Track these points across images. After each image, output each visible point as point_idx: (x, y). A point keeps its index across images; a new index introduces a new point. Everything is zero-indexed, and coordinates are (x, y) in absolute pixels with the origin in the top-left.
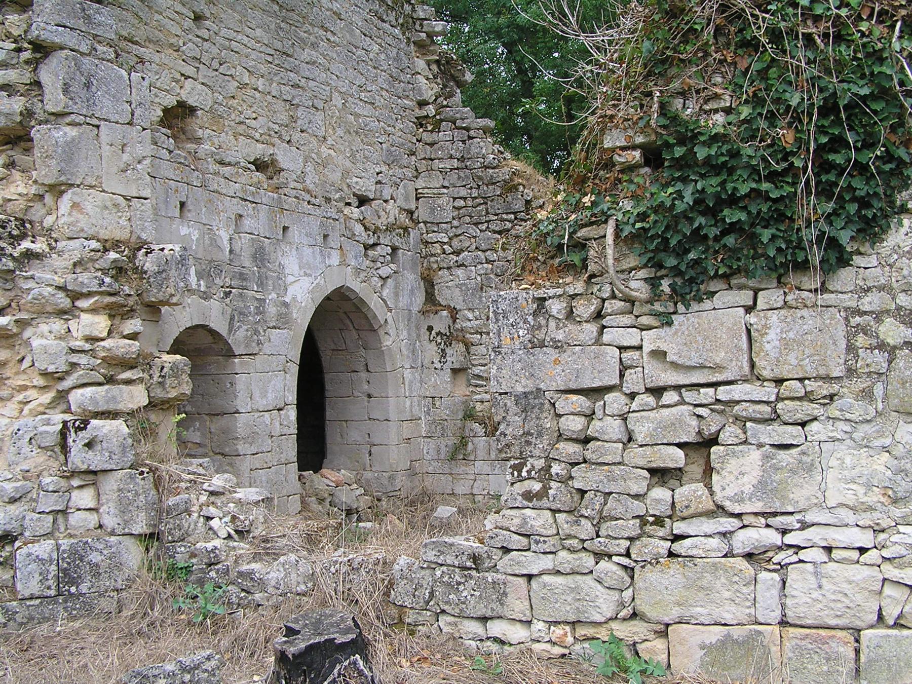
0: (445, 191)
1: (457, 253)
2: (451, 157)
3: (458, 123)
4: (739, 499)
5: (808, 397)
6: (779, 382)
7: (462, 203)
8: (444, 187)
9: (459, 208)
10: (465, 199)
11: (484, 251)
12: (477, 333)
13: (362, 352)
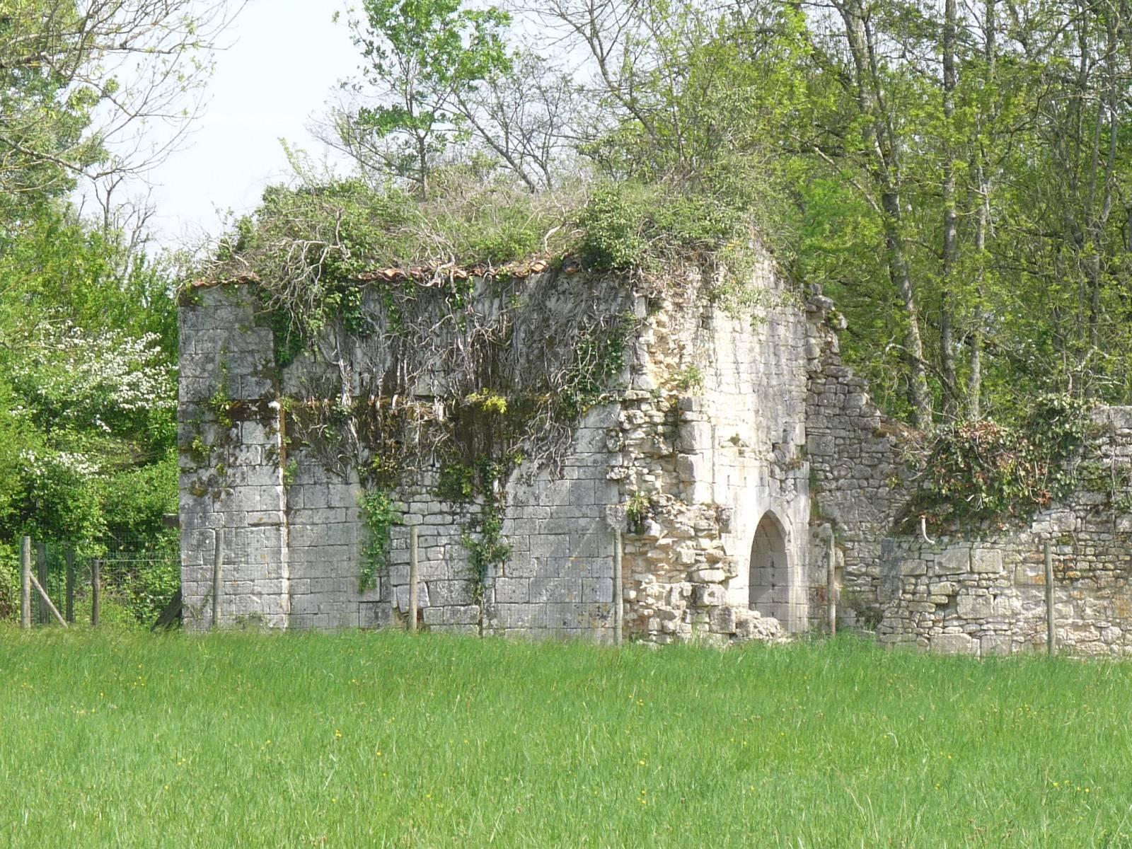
0: (828, 431)
1: (836, 479)
2: (834, 406)
3: (840, 379)
4: (966, 614)
5: (989, 579)
6: (979, 574)
7: (842, 441)
8: (828, 428)
9: (838, 445)
10: (844, 438)
11: (858, 479)
12: (850, 541)
13: (770, 553)
